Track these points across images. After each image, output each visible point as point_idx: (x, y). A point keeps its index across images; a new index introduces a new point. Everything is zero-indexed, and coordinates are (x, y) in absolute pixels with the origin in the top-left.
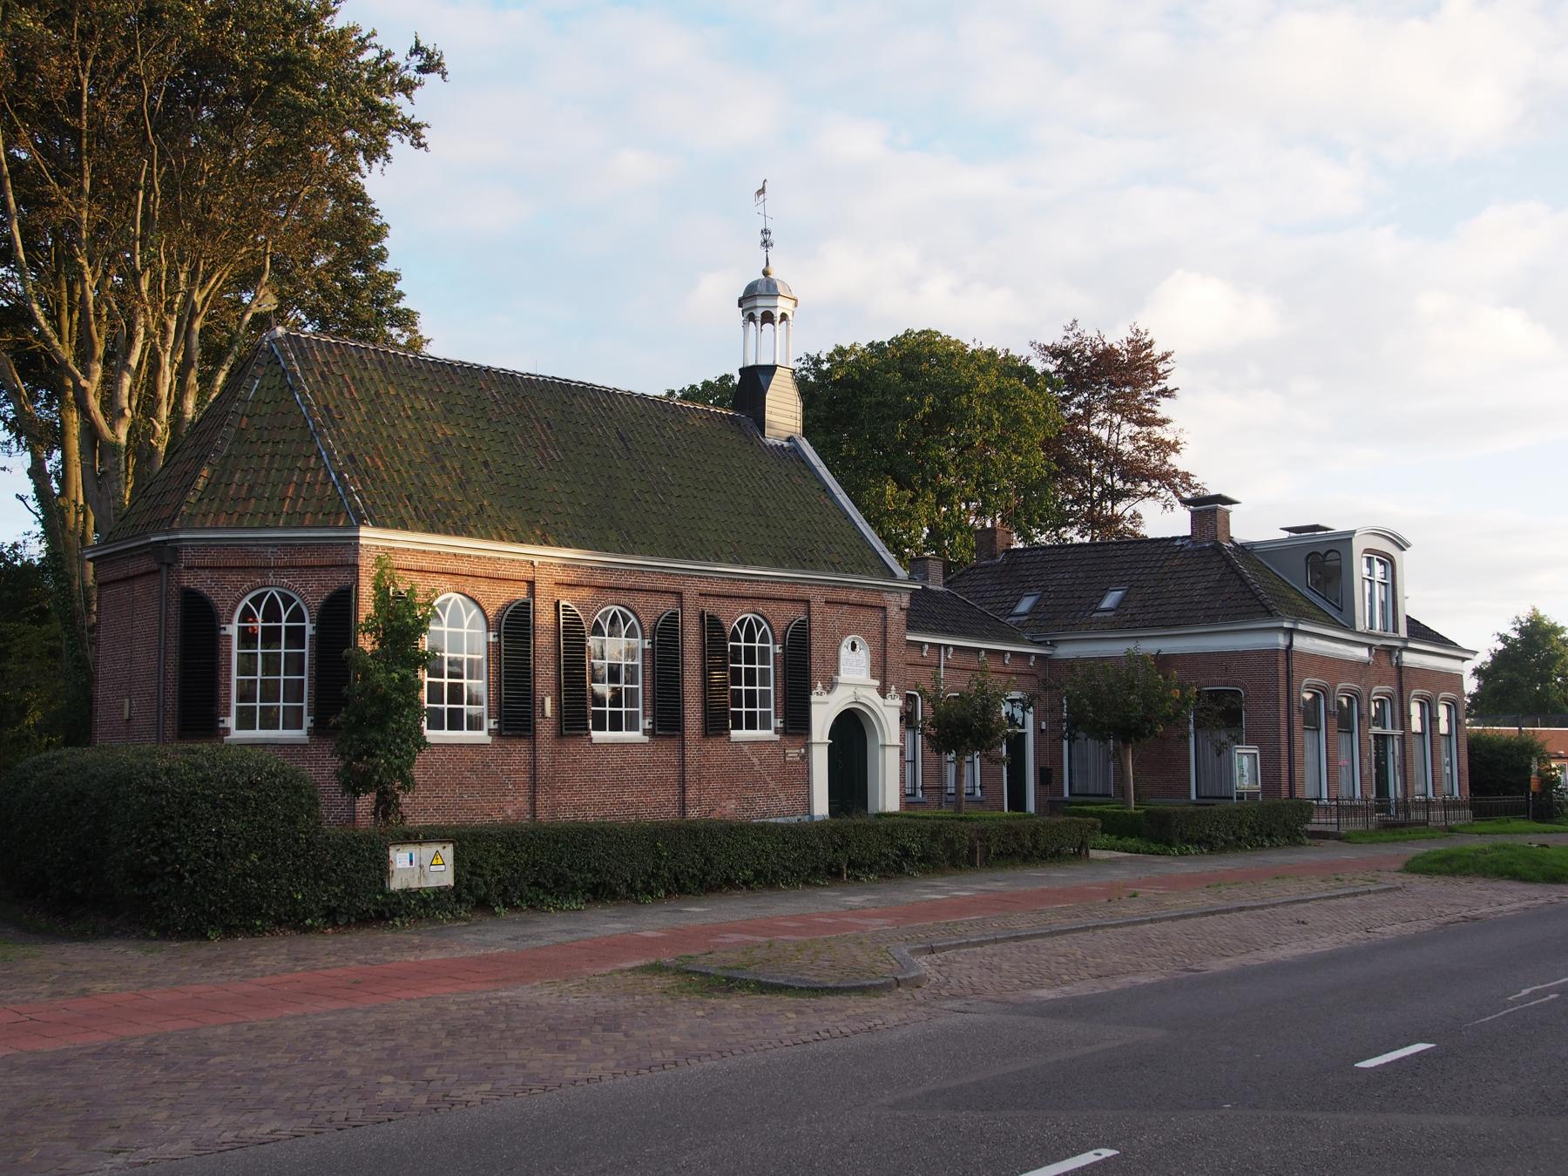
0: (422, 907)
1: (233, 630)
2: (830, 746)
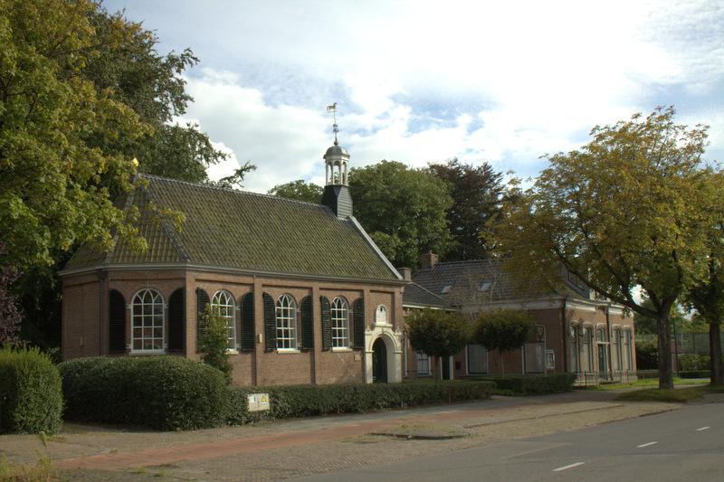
0: (255, 418)
1: (131, 306)
2: (373, 353)
